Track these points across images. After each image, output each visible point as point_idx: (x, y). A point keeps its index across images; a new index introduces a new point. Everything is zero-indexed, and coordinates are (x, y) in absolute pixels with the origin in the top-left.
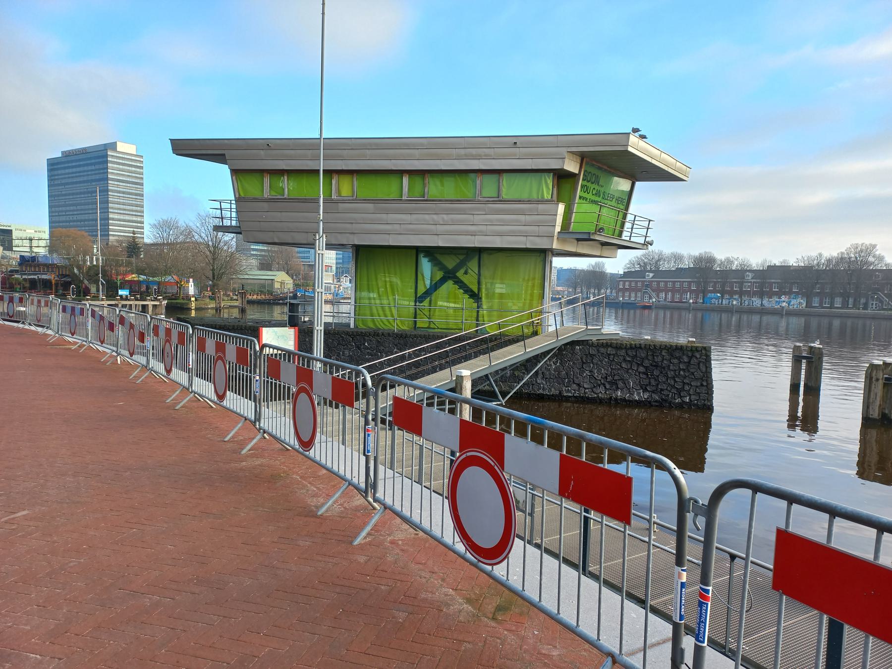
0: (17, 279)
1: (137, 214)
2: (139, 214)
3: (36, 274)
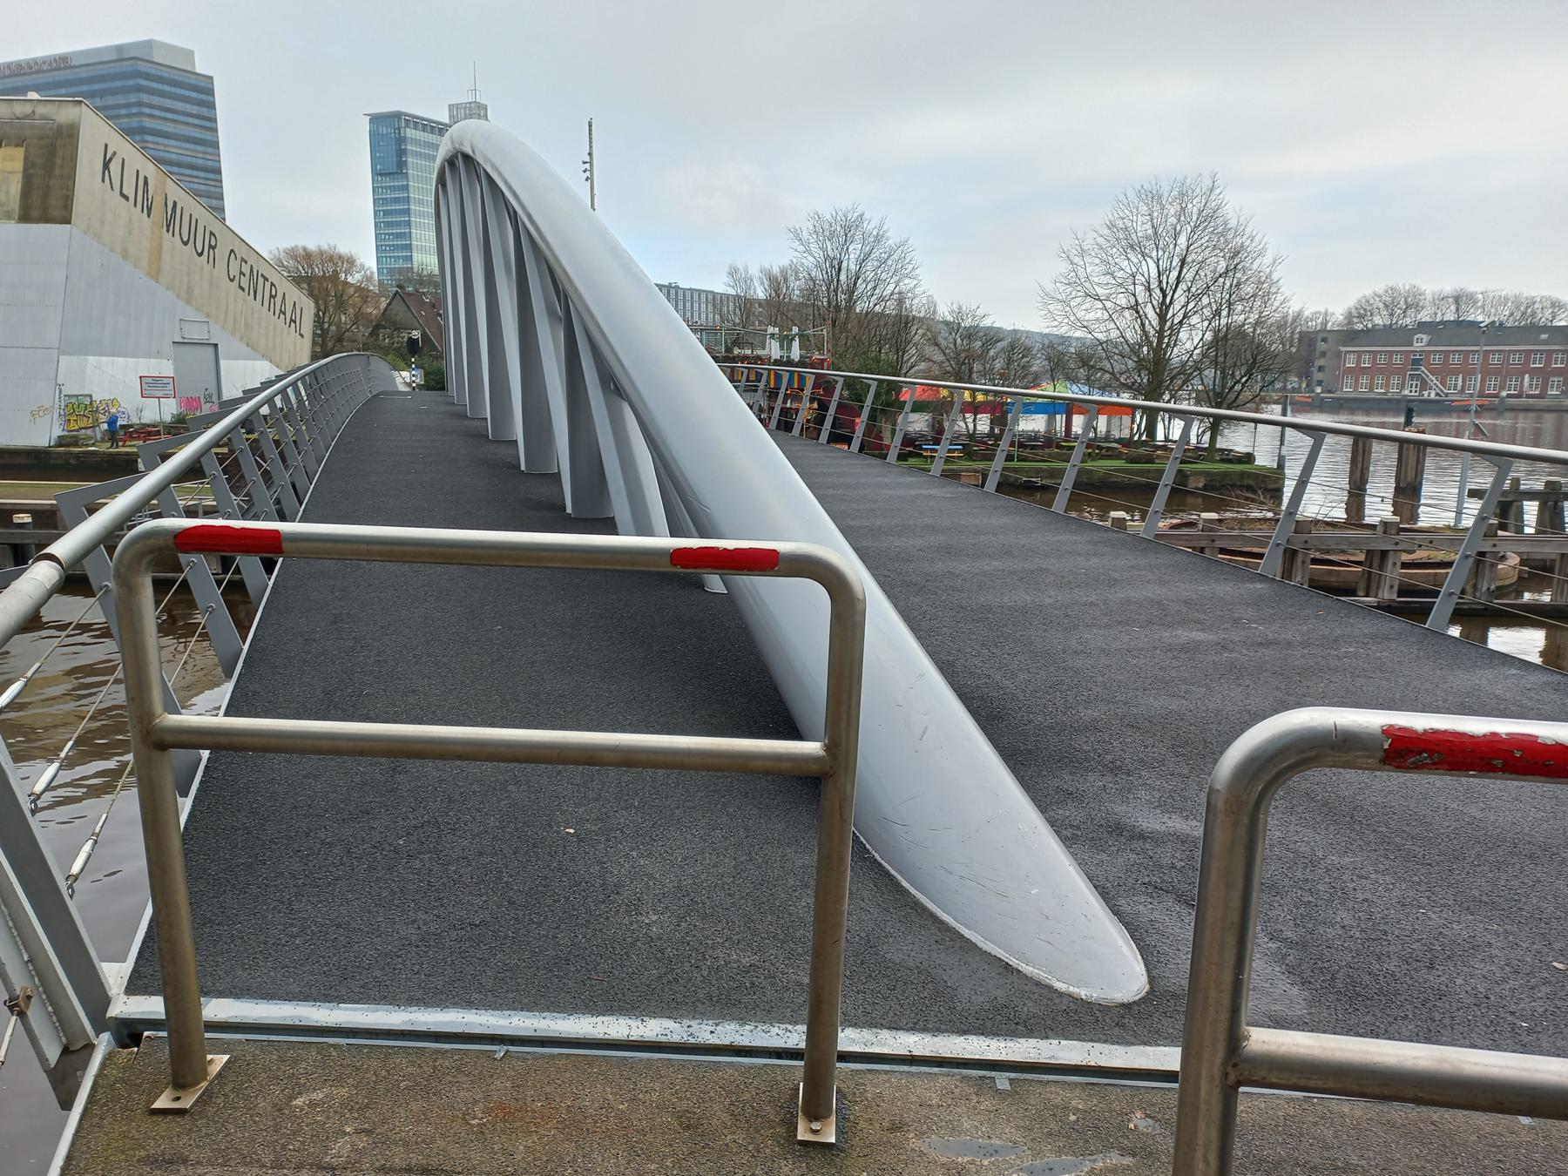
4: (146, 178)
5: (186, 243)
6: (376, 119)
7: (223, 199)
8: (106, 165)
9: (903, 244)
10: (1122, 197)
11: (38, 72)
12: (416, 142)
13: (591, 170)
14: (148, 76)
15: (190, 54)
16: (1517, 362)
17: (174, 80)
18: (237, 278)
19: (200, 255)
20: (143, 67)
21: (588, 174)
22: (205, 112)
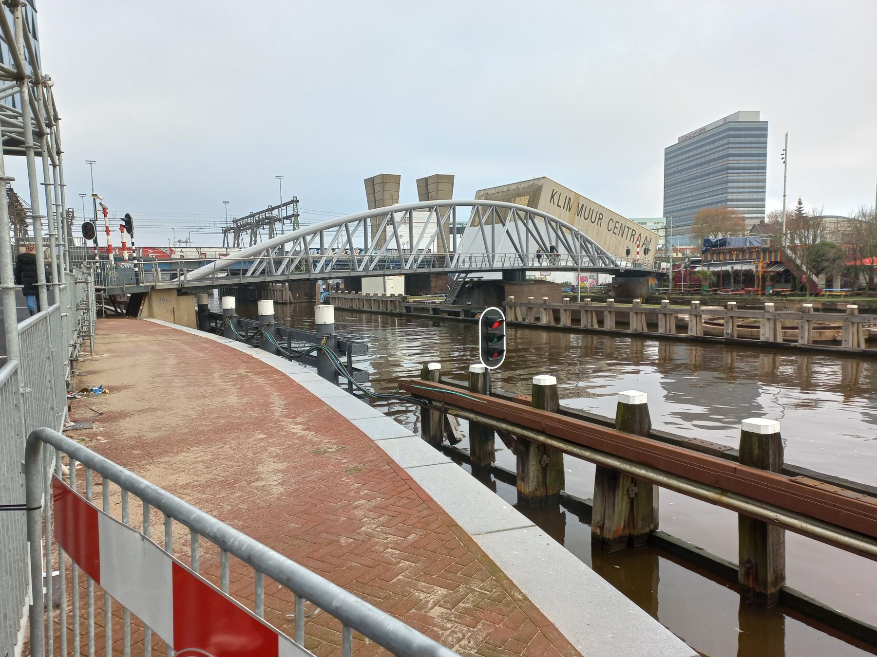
0: (703, 273)
1: (758, 190)
2: (760, 190)
3: (725, 265)
4: (570, 198)
8: (552, 197)
14: (734, 129)
16: (734, 261)
20: (732, 125)
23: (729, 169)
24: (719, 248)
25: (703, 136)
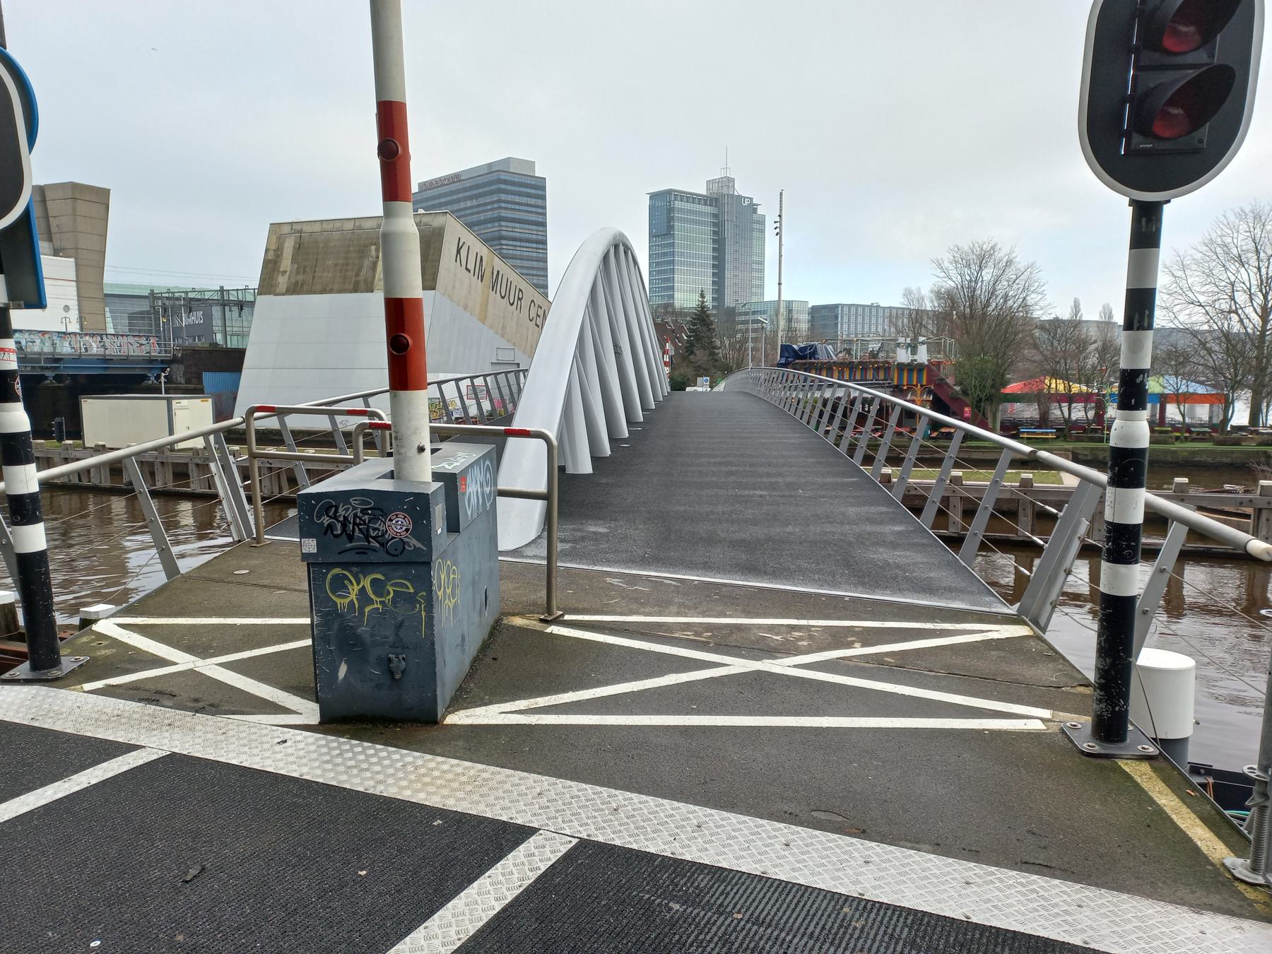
4: (481, 257)
5: (503, 298)
6: (654, 197)
7: (547, 262)
8: (458, 251)
9: (1032, 266)
10: (1222, 219)
11: (442, 185)
12: (682, 211)
13: (780, 228)
14: (505, 182)
15: (531, 164)
17: (524, 183)
18: (535, 319)
19: (512, 304)
20: (503, 176)
21: (778, 230)
22: (539, 202)
23: (501, 238)
24: (808, 361)
25: (453, 187)
